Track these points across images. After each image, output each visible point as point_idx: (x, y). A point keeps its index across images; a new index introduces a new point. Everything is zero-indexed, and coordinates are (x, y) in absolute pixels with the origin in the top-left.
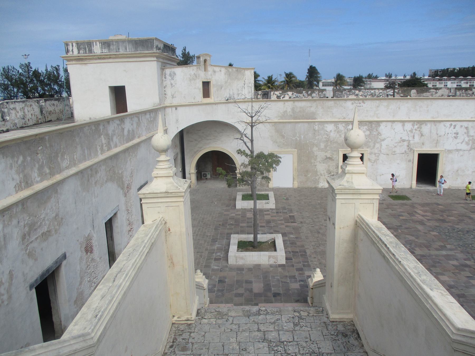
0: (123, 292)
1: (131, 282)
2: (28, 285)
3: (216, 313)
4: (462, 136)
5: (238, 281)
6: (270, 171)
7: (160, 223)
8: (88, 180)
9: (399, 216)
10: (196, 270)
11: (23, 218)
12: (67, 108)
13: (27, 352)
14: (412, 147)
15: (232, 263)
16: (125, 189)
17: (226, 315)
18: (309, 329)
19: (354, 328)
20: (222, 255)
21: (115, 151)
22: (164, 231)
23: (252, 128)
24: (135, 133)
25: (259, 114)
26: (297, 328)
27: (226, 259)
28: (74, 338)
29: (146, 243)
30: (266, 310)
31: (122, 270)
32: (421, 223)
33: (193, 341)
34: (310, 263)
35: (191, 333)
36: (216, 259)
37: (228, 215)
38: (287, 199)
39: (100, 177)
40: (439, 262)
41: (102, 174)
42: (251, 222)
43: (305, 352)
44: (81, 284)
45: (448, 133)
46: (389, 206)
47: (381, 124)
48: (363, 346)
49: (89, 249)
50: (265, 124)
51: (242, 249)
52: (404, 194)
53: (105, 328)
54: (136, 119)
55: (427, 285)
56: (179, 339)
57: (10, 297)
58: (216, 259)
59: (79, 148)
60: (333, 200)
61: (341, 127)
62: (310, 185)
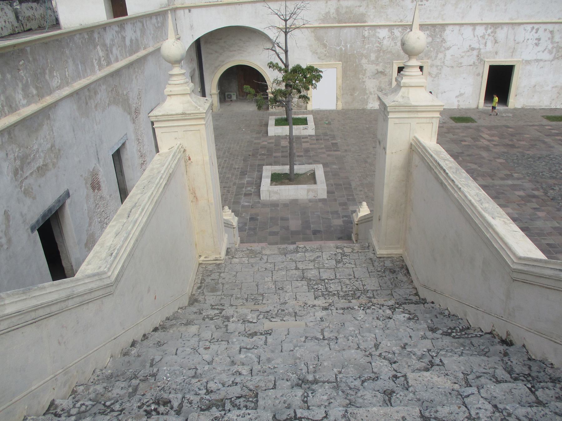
0: (140, 229)
1: (148, 217)
2: (28, 227)
3: (248, 252)
4: (545, 43)
5: (271, 218)
6: (308, 89)
7: (178, 150)
8: (87, 104)
9: (462, 141)
10: (223, 207)
11: (12, 149)
12: (49, 12)
13: (35, 290)
14: (482, 57)
15: (265, 199)
16: (133, 113)
17: (259, 253)
18: (353, 266)
19: (404, 264)
20: (253, 190)
21: (116, 66)
22: (183, 160)
23: (286, 35)
24: (140, 42)
25: (294, 17)
26: (340, 265)
27: (258, 194)
28: (89, 277)
29: (163, 174)
30: (305, 247)
31: (137, 205)
32: (487, 149)
33: (224, 281)
34: (356, 197)
35: (220, 273)
36: (246, 195)
37: (259, 144)
38: (329, 124)
39: (101, 99)
40: (503, 193)
41: (103, 95)
42: (287, 151)
43: (348, 290)
44: (90, 225)
45: (528, 39)
46: (450, 130)
47: (446, 28)
48: (412, 282)
49: (95, 186)
50: (303, 30)
51: (277, 182)
52: (468, 115)
53: (123, 266)
54: (139, 25)
55: (489, 213)
56: (208, 280)
57: (9, 241)
58: (246, 195)
59: (70, 62)
60: (384, 120)
61: (397, 32)
62: (357, 106)
